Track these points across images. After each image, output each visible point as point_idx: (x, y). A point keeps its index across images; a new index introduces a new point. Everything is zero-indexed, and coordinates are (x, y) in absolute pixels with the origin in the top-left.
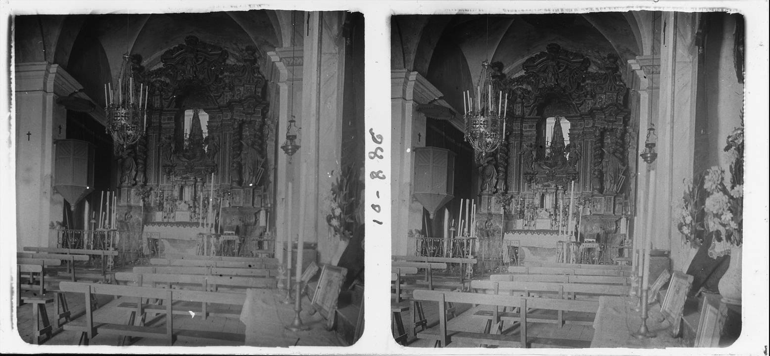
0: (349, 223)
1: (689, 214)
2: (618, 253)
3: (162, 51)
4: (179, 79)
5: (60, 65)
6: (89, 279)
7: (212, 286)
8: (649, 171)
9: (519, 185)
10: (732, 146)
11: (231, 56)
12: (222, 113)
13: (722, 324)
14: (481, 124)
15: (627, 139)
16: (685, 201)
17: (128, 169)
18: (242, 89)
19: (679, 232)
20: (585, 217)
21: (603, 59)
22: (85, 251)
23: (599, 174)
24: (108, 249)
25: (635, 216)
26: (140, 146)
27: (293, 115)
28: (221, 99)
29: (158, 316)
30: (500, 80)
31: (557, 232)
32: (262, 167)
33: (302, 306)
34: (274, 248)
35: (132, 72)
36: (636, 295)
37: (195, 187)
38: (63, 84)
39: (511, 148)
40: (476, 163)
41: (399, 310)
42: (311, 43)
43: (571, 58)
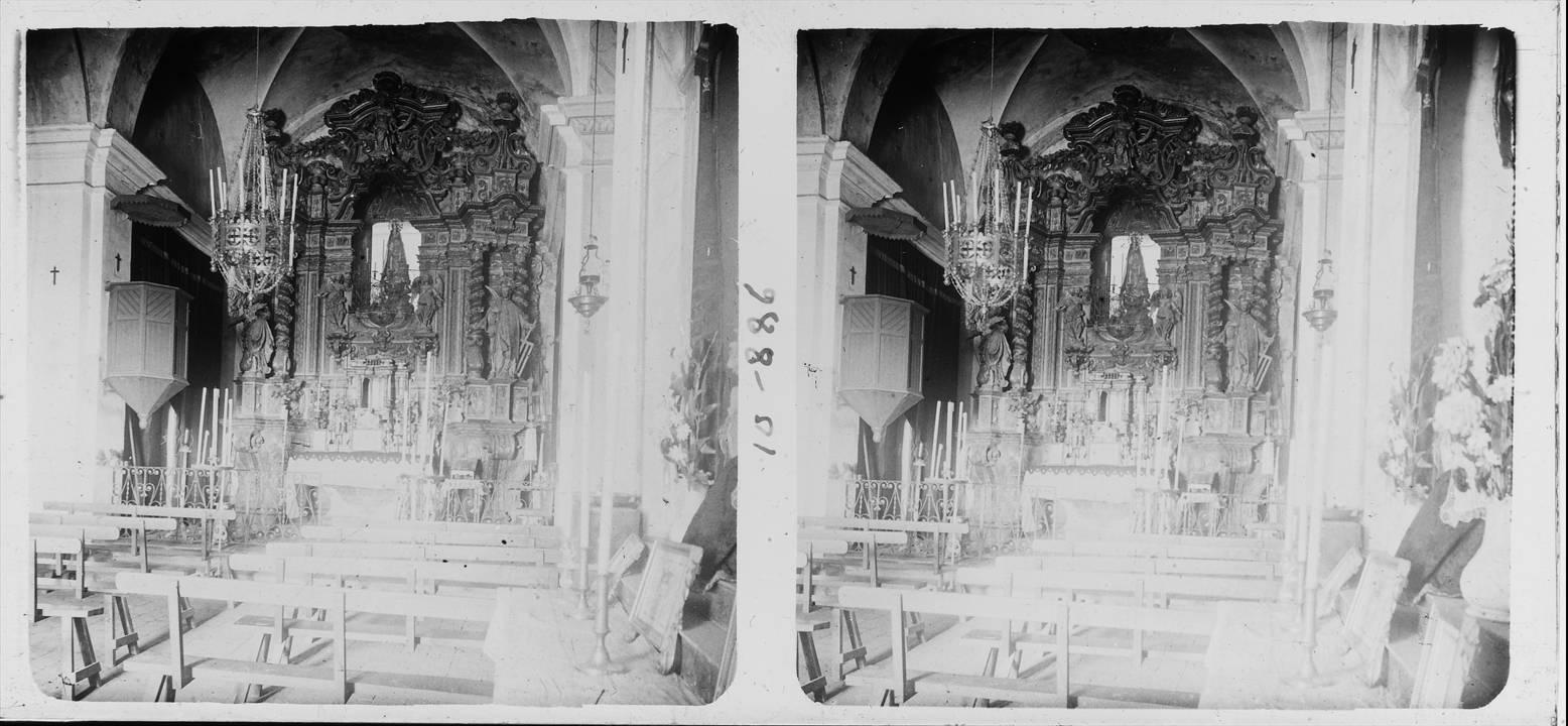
0: (705, 455)
1: (1402, 436)
2: (1256, 513)
3: (1067, 115)
4: (1100, 173)
5: (118, 130)
6: (176, 568)
7: (426, 582)
8: (1320, 346)
9: (1055, 374)
10: (1489, 296)
11: (468, 114)
12: (449, 230)
13: (1468, 659)
14: (979, 249)
15: (537, 267)
16: (1395, 408)
17: (256, 343)
18: (489, 180)
19: (1381, 471)
20: (1190, 440)
21: (1228, 119)
22: (167, 509)
23: (1218, 353)
24: (214, 507)
25: (1291, 437)
26: (1018, 309)
27: (594, 234)
28: (447, 200)
29: (317, 643)
30: (1018, 160)
31: (1134, 468)
32: (1267, 354)
33: (610, 625)
34: (553, 505)
35: (266, 145)
36: (1292, 600)
37: (393, 381)
38: (125, 170)
39: (1039, 298)
40: (231, 314)
41: (809, 628)
42: (629, 82)
43: (424, 101)
